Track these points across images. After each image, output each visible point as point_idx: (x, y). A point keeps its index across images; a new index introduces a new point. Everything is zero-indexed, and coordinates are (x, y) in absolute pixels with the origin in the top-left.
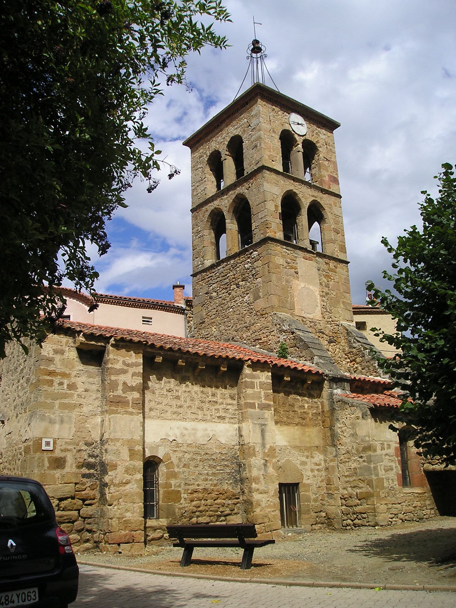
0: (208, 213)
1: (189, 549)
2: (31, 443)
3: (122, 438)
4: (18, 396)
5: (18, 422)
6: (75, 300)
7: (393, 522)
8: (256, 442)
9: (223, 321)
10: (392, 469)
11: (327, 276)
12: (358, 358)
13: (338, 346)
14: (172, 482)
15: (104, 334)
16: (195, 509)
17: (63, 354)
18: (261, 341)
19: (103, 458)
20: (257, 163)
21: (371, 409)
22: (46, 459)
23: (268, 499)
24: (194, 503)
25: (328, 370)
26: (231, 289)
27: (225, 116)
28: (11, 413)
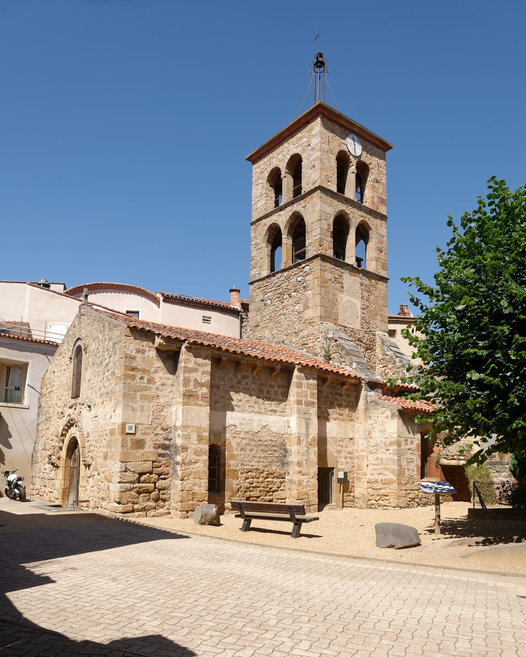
0: (267, 227)
1: (248, 519)
2: (117, 427)
3: (193, 425)
4: (104, 386)
5: (104, 408)
6: (143, 298)
7: (411, 505)
8: (301, 433)
9: (275, 326)
10: (413, 462)
11: (369, 291)
12: (390, 365)
13: (373, 353)
14: (231, 462)
15: (178, 337)
16: (249, 485)
17: (144, 353)
18: (307, 346)
19: (176, 441)
20: (314, 183)
21: (400, 412)
22: (129, 441)
23: (308, 480)
24: (248, 481)
25: (365, 375)
26: (284, 298)
27: (286, 134)
28: (98, 400)
